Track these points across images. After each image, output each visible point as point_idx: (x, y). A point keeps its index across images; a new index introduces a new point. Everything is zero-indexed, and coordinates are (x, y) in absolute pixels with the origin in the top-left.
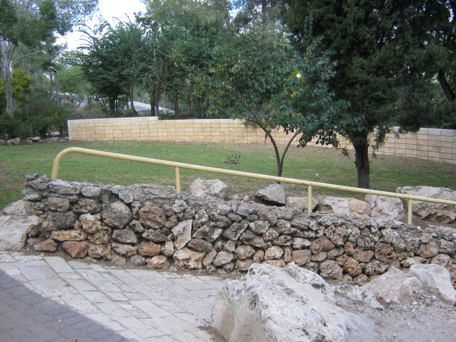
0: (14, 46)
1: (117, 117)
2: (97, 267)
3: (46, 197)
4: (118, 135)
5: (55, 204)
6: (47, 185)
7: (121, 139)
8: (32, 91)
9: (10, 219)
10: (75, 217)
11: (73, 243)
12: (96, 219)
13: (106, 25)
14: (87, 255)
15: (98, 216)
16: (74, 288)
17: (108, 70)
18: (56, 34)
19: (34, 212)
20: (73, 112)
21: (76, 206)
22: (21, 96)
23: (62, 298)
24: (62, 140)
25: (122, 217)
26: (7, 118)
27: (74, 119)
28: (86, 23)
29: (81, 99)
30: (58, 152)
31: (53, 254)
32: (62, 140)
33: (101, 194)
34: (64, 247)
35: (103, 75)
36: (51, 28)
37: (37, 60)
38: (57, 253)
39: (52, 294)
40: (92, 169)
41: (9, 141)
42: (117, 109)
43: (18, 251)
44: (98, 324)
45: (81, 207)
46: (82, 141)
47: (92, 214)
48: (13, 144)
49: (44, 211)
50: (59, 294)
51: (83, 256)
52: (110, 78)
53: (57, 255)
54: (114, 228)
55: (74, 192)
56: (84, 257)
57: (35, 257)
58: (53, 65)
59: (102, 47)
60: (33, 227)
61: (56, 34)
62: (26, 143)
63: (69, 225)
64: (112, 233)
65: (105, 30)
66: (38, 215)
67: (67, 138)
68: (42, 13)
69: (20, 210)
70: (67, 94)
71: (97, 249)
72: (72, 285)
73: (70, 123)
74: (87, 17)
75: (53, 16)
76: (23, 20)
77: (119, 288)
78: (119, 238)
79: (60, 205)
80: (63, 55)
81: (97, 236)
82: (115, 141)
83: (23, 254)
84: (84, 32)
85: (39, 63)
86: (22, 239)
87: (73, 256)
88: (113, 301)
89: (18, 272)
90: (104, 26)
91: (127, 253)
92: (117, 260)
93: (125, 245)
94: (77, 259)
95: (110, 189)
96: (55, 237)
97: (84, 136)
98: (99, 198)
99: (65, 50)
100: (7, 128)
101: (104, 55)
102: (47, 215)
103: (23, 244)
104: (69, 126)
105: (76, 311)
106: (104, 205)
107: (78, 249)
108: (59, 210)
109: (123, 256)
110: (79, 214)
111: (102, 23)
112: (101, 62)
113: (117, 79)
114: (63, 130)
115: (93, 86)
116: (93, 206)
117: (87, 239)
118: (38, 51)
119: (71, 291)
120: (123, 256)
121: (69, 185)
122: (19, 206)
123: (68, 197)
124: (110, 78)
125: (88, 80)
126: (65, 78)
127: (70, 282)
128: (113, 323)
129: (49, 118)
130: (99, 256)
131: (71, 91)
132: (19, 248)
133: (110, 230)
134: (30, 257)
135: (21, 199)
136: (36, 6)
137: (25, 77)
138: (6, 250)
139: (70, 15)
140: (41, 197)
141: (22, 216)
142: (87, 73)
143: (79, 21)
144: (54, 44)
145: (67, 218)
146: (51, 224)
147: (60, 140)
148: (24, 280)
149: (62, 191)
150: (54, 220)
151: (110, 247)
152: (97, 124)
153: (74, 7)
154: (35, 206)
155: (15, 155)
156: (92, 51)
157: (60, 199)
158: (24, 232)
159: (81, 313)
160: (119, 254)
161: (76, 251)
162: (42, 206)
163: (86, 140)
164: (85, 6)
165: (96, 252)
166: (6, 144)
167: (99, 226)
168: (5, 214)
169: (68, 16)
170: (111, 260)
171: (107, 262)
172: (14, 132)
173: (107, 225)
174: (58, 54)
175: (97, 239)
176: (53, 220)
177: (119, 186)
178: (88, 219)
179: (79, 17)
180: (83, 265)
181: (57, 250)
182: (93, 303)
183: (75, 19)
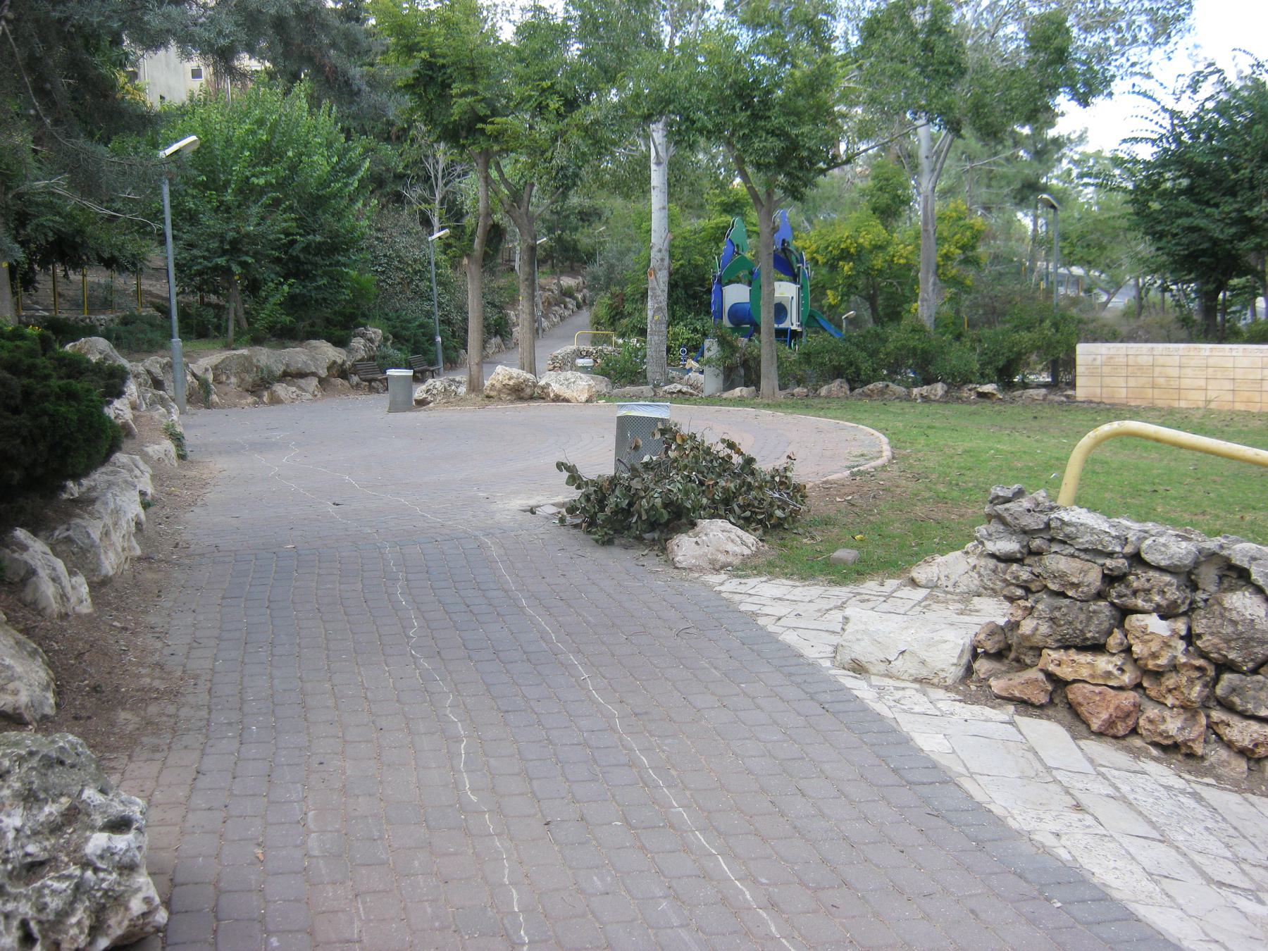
0: (952, 141)
1: (1220, 342)
2: (1160, 773)
3: (1038, 553)
4: (1220, 396)
5: (1063, 575)
6: (1046, 519)
7: (1227, 407)
8: (985, 260)
9: (926, 599)
10: (1113, 617)
11: (1097, 689)
12: (1174, 632)
13: (1212, 73)
14: (1134, 731)
15: (1181, 626)
16: (1096, 819)
17: (1207, 204)
18: (1063, 101)
19: (1002, 589)
20: (1093, 321)
21: (1120, 588)
22: (954, 271)
23: (1064, 841)
24: (1057, 398)
25: (1252, 639)
26: (918, 329)
27: (1095, 340)
28: (1153, 70)
29: (1115, 286)
30: (1080, 434)
31: (1038, 712)
32: (1057, 398)
33: (1197, 564)
34: (1070, 696)
35: (1190, 219)
36: (1054, 90)
37: (1003, 177)
38: (1050, 713)
39: (1034, 825)
40: (1147, 488)
41: (915, 391)
42: (1223, 319)
43: (947, 688)
44: (1166, 941)
45: (1135, 593)
46: (1112, 405)
47: (1163, 617)
48: (925, 399)
49: (1028, 590)
50: (1055, 827)
51: (1121, 733)
52: (1212, 226)
53: (1049, 718)
54: (1225, 666)
55: (1118, 549)
56: (1124, 737)
57: (988, 712)
58: (1045, 189)
59: (1194, 136)
60: (994, 631)
61: (1063, 101)
62: (958, 398)
63: (1093, 638)
64: (1216, 680)
65: (1207, 89)
66: (1011, 599)
67: (1070, 392)
68: (1032, 47)
69: (954, 578)
70: (1077, 271)
71: (1164, 720)
72: (1091, 810)
73: (1086, 353)
74: (1158, 53)
75: (1061, 55)
76: (982, 68)
77: (1228, 846)
78: (1237, 700)
79: (1075, 580)
80: (1072, 161)
81: (1170, 681)
82: (1211, 412)
83: (958, 697)
84: (1145, 95)
85: (1009, 184)
86: (960, 657)
87: (1095, 727)
88: (1210, 880)
89: (945, 746)
90: (1206, 77)
91: (1256, 745)
92: (1222, 763)
93: (1252, 722)
94: (1105, 739)
95: (1225, 553)
96: (1051, 668)
97: (1120, 391)
98: (1190, 573)
99: (1080, 149)
100: (915, 355)
101: (1199, 160)
102: (1037, 602)
103: (960, 672)
104: (1080, 359)
105: (1104, 889)
106: (1200, 596)
107: (1111, 710)
108: (1070, 593)
109: (1243, 752)
110: (1124, 612)
111: (1200, 67)
112: (1185, 182)
113: (1233, 230)
114: (1063, 370)
115: (1158, 249)
116: (1168, 596)
117: (1138, 686)
118: (1008, 153)
119: (1089, 827)
120: (1243, 752)
121: (1105, 527)
122: (953, 566)
123: (1101, 561)
124: (1212, 226)
125: (1146, 233)
126: (1075, 229)
127: (1085, 800)
128: (1213, 946)
129: (1025, 335)
130: (1169, 742)
131: (1089, 263)
132: (949, 682)
133: (1211, 672)
134: (976, 708)
135: (954, 549)
136: (1016, 29)
137: (967, 221)
138: (916, 680)
139: (1109, 48)
140: (1025, 551)
141: (957, 594)
142: (1142, 212)
143: (1133, 65)
144: (1051, 133)
145: (1089, 619)
146: (1044, 628)
147: (1051, 397)
148: (961, 770)
149: (1084, 540)
150: (1052, 619)
151: (1204, 721)
152: (1161, 360)
153: (1120, 27)
154: (1005, 573)
155: (933, 427)
156: (1166, 150)
157: (1077, 564)
158: (968, 641)
159: (1116, 895)
160: (1229, 745)
161: (1104, 716)
162: (1025, 575)
163: (1124, 401)
164: (1153, 21)
165: (1162, 727)
166: (908, 398)
167: (1180, 655)
168: (914, 583)
169: (1101, 53)
170: (1202, 758)
171: (1191, 762)
172: (931, 369)
173: (1203, 655)
174: (1059, 160)
175: (1170, 691)
176: (1051, 619)
177: (1253, 546)
178: (1149, 630)
179: (1135, 53)
180: (1122, 758)
181: (1051, 701)
182: (1151, 874)
183: (1123, 60)
